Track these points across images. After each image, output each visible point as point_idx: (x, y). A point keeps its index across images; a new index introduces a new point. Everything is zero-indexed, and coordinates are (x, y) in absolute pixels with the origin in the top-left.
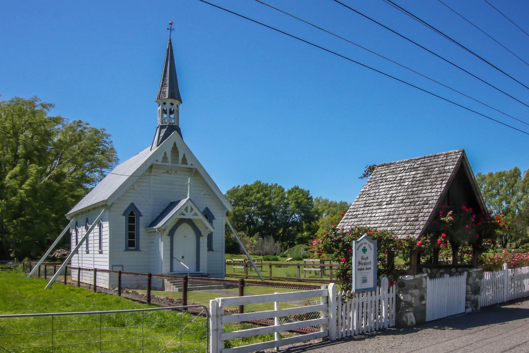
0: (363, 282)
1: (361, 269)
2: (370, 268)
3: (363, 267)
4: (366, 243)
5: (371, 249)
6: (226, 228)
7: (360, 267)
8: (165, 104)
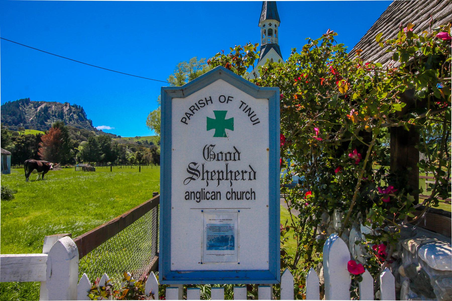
0: (210, 247)
1: (201, 196)
2: (251, 194)
3: (213, 186)
4: (229, 99)
5: (256, 122)
6: (22, 101)
7: (198, 185)
8: (264, 26)
